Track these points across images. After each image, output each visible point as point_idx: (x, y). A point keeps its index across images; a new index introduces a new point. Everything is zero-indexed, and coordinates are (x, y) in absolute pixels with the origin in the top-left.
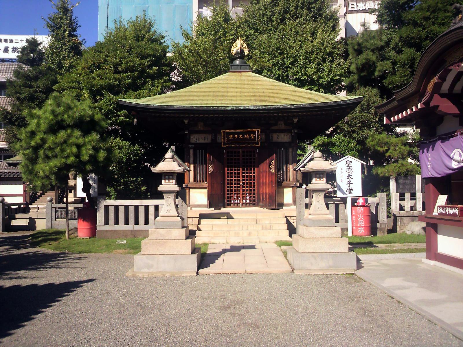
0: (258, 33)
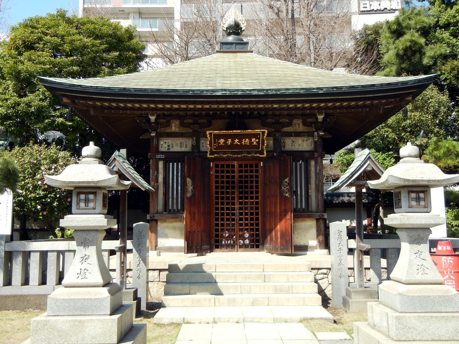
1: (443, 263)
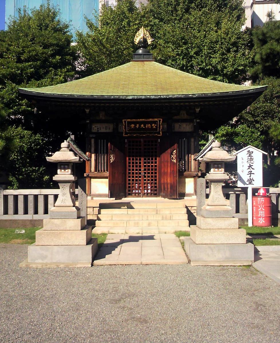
0: (163, 23)
1: (259, 201)
